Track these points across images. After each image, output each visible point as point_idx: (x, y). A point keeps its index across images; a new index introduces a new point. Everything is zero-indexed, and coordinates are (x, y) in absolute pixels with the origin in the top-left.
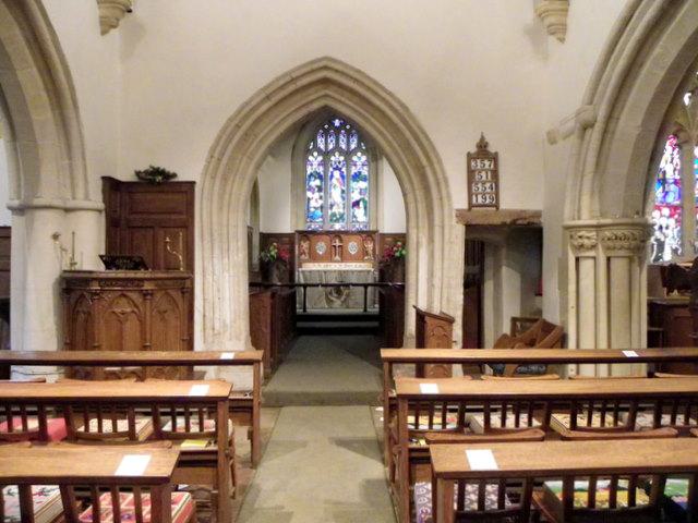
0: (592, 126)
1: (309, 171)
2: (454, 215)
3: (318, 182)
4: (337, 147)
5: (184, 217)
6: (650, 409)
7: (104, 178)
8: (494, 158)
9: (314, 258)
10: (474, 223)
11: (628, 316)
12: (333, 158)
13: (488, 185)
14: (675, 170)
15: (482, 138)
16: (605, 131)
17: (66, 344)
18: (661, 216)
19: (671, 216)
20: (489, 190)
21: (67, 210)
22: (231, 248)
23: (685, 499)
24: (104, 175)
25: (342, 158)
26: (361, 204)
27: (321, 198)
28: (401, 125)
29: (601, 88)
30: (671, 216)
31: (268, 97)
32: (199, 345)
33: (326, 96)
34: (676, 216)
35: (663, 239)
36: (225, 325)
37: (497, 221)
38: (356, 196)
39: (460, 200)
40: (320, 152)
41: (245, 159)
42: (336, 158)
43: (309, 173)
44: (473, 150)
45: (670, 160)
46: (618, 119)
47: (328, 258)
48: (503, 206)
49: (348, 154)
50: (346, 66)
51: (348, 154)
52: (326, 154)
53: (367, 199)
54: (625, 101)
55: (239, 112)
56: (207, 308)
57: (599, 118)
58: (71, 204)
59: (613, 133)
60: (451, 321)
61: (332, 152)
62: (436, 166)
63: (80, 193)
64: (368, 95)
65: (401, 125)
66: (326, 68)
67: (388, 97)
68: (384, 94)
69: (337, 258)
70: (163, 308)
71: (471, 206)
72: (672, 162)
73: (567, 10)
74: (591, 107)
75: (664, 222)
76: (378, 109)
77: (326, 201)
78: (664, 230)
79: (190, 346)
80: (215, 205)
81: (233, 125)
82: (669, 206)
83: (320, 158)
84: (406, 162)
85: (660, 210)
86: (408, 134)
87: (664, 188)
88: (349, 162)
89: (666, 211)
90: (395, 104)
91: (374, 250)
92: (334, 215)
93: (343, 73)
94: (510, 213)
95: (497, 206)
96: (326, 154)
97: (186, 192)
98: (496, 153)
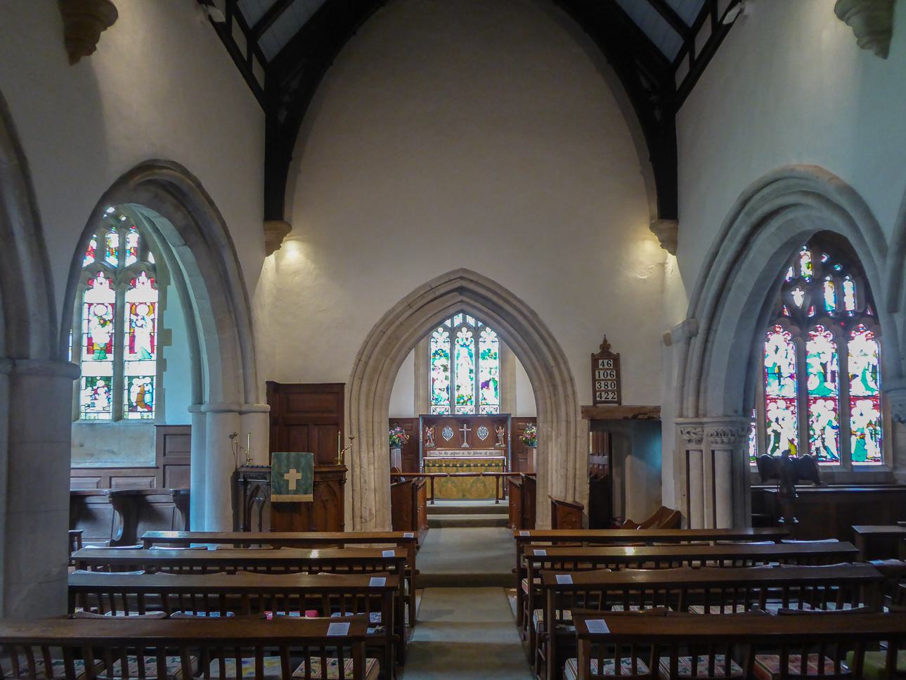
0: (696, 336)
1: (434, 348)
2: (579, 410)
3: (444, 361)
4: (465, 324)
5: (334, 415)
6: (780, 603)
8: (616, 359)
9: (440, 443)
10: (598, 418)
11: (685, 498)
12: (459, 334)
14: (790, 364)
15: (605, 341)
16: (706, 341)
17: (596, 477)
19: (787, 408)
21: (241, 413)
22: (376, 442)
25: (470, 334)
26: (491, 384)
27: (446, 378)
30: (787, 408)
31: (410, 306)
32: (348, 528)
33: (462, 301)
34: (792, 408)
36: (370, 514)
37: (619, 416)
38: (483, 377)
39: (585, 399)
41: (388, 360)
42: (464, 335)
43: (433, 352)
44: (597, 351)
46: (716, 331)
47: (456, 444)
48: (625, 403)
49: (476, 333)
50: (480, 276)
51: (476, 333)
52: (453, 332)
53: (497, 379)
54: (720, 316)
55: (383, 320)
56: (356, 499)
57: (699, 332)
58: (245, 408)
60: (581, 508)
61: (459, 328)
62: (562, 366)
63: (252, 398)
64: (500, 302)
65: (531, 329)
66: (462, 278)
67: (518, 304)
68: (515, 302)
69: (465, 445)
70: (324, 498)
71: (595, 402)
72: (786, 357)
73: (677, 229)
74: (694, 320)
76: (508, 314)
77: (452, 381)
78: (780, 422)
79: (340, 527)
80: (363, 403)
81: (378, 330)
82: (784, 398)
83: (447, 334)
84: (537, 364)
85: (776, 402)
86: (536, 337)
87: (780, 382)
88: (477, 337)
89: (782, 404)
90: (525, 311)
91: (505, 437)
92: (461, 397)
93: (477, 283)
94: (631, 409)
95: (619, 402)
96: (453, 332)
97: (337, 393)
98: (618, 354)
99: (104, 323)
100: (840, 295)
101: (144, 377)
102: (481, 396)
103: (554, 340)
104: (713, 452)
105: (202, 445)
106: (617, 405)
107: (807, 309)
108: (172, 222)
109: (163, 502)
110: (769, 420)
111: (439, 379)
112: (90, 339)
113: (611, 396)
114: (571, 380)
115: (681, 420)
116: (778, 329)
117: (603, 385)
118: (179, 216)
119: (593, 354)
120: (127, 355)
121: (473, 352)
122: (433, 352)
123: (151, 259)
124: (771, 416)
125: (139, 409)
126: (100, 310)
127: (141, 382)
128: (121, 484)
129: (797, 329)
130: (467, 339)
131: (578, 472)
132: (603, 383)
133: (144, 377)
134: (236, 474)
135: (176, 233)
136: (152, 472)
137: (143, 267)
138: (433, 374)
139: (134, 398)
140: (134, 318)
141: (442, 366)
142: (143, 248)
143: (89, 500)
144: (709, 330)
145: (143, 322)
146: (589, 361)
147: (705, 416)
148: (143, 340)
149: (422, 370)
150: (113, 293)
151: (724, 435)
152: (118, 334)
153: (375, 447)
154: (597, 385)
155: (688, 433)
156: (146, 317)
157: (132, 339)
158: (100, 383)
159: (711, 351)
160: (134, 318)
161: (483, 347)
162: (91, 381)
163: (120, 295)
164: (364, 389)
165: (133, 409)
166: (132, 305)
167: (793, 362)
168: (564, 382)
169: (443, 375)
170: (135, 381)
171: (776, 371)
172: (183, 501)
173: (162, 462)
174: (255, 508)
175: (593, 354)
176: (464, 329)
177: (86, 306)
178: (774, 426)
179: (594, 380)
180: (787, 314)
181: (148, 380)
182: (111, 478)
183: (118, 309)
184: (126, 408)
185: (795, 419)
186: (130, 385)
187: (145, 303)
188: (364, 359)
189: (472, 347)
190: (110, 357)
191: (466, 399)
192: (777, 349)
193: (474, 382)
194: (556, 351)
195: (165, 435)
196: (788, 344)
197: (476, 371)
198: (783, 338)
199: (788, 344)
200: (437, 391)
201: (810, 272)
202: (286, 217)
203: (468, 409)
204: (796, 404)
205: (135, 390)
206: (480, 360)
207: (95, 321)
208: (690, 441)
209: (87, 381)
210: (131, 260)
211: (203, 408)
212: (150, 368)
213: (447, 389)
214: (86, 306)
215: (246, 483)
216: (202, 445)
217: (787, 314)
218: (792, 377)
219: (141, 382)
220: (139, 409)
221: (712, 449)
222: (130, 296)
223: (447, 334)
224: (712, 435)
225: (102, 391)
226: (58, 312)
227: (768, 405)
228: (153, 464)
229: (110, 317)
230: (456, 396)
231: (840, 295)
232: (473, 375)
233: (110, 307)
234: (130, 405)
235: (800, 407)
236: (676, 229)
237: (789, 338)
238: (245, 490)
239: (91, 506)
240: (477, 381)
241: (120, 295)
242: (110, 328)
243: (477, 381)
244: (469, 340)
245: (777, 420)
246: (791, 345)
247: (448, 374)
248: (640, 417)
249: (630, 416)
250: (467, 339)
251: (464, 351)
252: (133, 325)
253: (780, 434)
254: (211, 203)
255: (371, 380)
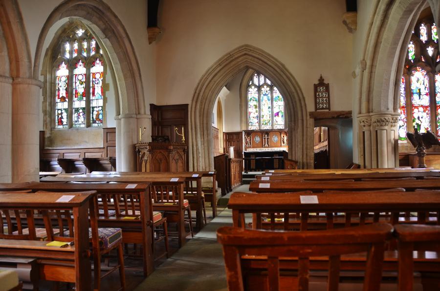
1: (250, 96)
4: (265, 84)
7: (150, 104)
8: (327, 87)
12: (263, 89)
13: (325, 99)
14: (426, 87)
15: (321, 77)
16: (371, 72)
18: (419, 111)
19: (424, 111)
20: (325, 102)
23: (36, 230)
24: (330, 85)
25: (268, 89)
26: (280, 114)
28: (282, 73)
29: (268, 66)
30: (424, 111)
31: (220, 65)
34: (427, 111)
35: (420, 124)
40: (256, 86)
42: (265, 89)
44: (317, 82)
45: (422, 83)
52: (259, 88)
55: (207, 72)
59: (375, 72)
61: (263, 86)
65: (282, 73)
71: (316, 109)
72: (424, 84)
74: (364, 61)
75: (420, 115)
78: (420, 119)
82: (422, 106)
85: (418, 109)
89: (421, 109)
92: (263, 121)
94: (336, 113)
95: (329, 108)
96: (259, 88)
98: (328, 84)
99: (81, 83)
100: (429, 34)
101: (99, 107)
102: (274, 120)
103: (294, 78)
104: (377, 131)
105: (120, 135)
106: (327, 110)
107: (435, 57)
108: (98, 26)
109: (106, 163)
110: (414, 118)
111: (252, 111)
112: (76, 91)
113: (325, 106)
114: (304, 98)
115: (360, 115)
116: (418, 69)
117: (321, 100)
118: (101, 23)
119: (315, 84)
120: (92, 97)
121: (270, 98)
122: (249, 98)
123: (101, 52)
124: (416, 116)
125: (97, 122)
126: (80, 77)
127: (97, 109)
128: (88, 155)
129: (429, 68)
130: (267, 91)
131: (308, 146)
132: (321, 99)
133: (99, 107)
134: (134, 147)
135: (101, 32)
136: (102, 150)
137: (98, 56)
138: (250, 110)
139: (95, 117)
140: (94, 79)
141: (254, 105)
142: (97, 49)
143: (76, 163)
144: (372, 66)
145: (98, 81)
146: (312, 88)
147: (372, 112)
148: (98, 90)
149: (244, 108)
150: (85, 69)
151: (378, 122)
152: (87, 88)
153: (205, 136)
154: (318, 100)
155: (363, 121)
156: (100, 79)
157: (94, 89)
158: (81, 111)
159: (374, 78)
160: (94, 79)
161: (275, 95)
162: (77, 110)
163: (88, 70)
164: (198, 107)
165: (94, 122)
166: (93, 74)
167: (428, 86)
168: (300, 100)
169: (254, 110)
170: (95, 109)
171: (418, 91)
172: (113, 162)
173: (106, 145)
174: (144, 164)
175: (315, 84)
176: (265, 87)
177: (74, 76)
178: (417, 121)
179: (316, 98)
180: (424, 61)
181: (100, 108)
182: (85, 153)
183: (87, 76)
184: (92, 122)
185: (428, 117)
186: (93, 111)
187: (99, 73)
188: (197, 92)
189: (269, 95)
190: (84, 98)
191: (267, 122)
192: (418, 80)
193: (271, 113)
194: (295, 83)
195: (107, 133)
196: (425, 77)
197: (272, 107)
198: (421, 74)
199: (425, 77)
200: (252, 118)
201: (437, 37)
202: (158, 26)
203: (268, 127)
204: (429, 109)
205: (95, 113)
206: (274, 102)
207: (78, 83)
208: (364, 126)
209: (75, 110)
210: (93, 53)
211: (120, 117)
212: (101, 103)
213: (257, 117)
214: (74, 76)
215: (139, 152)
216: (120, 135)
217: (424, 61)
218: (427, 94)
219: (97, 109)
220: (97, 122)
221: (376, 129)
222: (93, 70)
223: (256, 89)
224: (375, 122)
225: (81, 114)
226: (32, 56)
227: (413, 110)
228: (102, 146)
229: (84, 80)
230: (262, 121)
231: (429, 34)
232: (270, 110)
233: (84, 76)
234: (93, 120)
235: (431, 111)
236: (356, 16)
237: (425, 74)
238: (139, 155)
239: (77, 166)
240: (272, 112)
241: (88, 70)
242: (84, 85)
243: (272, 112)
244: (268, 92)
245: (419, 118)
246: (426, 78)
247: (257, 109)
248: (341, 116)
249: (336, 116)
250: (267, 91)
251: (265, 98)
252: (94, 83)
253: (420, 125)
254: (116, 17)
255: (201, 103)
